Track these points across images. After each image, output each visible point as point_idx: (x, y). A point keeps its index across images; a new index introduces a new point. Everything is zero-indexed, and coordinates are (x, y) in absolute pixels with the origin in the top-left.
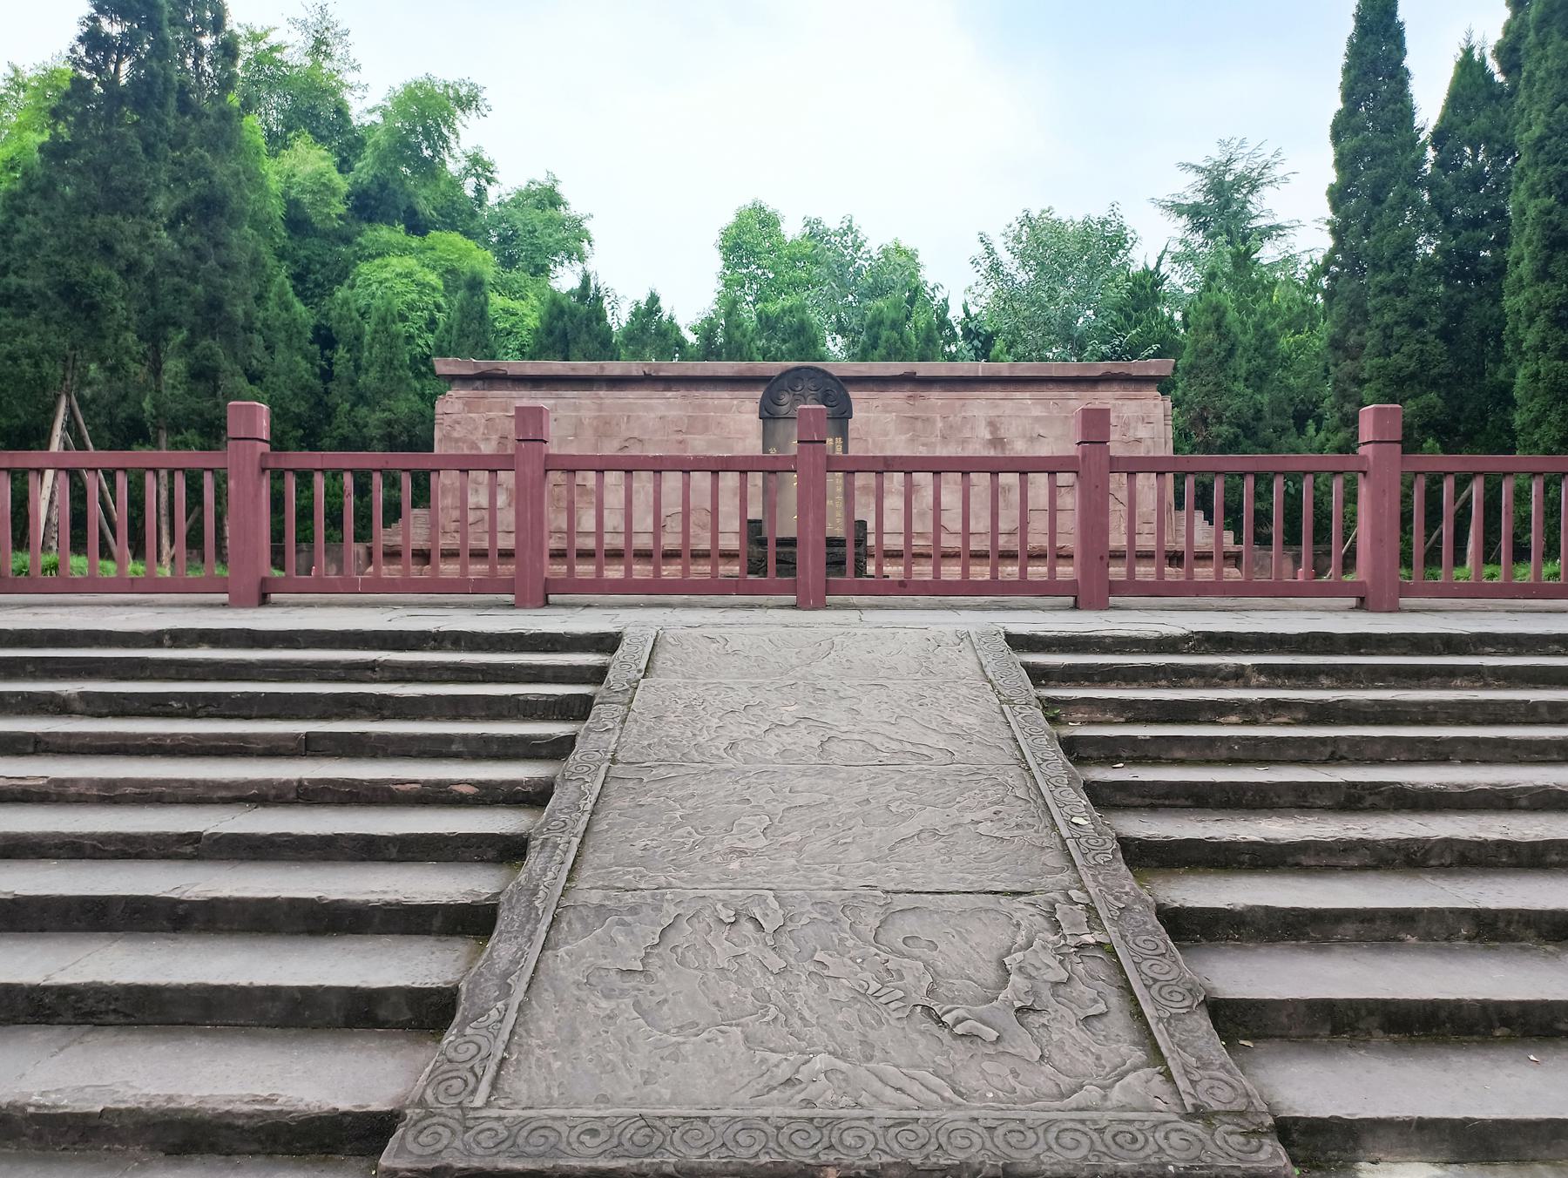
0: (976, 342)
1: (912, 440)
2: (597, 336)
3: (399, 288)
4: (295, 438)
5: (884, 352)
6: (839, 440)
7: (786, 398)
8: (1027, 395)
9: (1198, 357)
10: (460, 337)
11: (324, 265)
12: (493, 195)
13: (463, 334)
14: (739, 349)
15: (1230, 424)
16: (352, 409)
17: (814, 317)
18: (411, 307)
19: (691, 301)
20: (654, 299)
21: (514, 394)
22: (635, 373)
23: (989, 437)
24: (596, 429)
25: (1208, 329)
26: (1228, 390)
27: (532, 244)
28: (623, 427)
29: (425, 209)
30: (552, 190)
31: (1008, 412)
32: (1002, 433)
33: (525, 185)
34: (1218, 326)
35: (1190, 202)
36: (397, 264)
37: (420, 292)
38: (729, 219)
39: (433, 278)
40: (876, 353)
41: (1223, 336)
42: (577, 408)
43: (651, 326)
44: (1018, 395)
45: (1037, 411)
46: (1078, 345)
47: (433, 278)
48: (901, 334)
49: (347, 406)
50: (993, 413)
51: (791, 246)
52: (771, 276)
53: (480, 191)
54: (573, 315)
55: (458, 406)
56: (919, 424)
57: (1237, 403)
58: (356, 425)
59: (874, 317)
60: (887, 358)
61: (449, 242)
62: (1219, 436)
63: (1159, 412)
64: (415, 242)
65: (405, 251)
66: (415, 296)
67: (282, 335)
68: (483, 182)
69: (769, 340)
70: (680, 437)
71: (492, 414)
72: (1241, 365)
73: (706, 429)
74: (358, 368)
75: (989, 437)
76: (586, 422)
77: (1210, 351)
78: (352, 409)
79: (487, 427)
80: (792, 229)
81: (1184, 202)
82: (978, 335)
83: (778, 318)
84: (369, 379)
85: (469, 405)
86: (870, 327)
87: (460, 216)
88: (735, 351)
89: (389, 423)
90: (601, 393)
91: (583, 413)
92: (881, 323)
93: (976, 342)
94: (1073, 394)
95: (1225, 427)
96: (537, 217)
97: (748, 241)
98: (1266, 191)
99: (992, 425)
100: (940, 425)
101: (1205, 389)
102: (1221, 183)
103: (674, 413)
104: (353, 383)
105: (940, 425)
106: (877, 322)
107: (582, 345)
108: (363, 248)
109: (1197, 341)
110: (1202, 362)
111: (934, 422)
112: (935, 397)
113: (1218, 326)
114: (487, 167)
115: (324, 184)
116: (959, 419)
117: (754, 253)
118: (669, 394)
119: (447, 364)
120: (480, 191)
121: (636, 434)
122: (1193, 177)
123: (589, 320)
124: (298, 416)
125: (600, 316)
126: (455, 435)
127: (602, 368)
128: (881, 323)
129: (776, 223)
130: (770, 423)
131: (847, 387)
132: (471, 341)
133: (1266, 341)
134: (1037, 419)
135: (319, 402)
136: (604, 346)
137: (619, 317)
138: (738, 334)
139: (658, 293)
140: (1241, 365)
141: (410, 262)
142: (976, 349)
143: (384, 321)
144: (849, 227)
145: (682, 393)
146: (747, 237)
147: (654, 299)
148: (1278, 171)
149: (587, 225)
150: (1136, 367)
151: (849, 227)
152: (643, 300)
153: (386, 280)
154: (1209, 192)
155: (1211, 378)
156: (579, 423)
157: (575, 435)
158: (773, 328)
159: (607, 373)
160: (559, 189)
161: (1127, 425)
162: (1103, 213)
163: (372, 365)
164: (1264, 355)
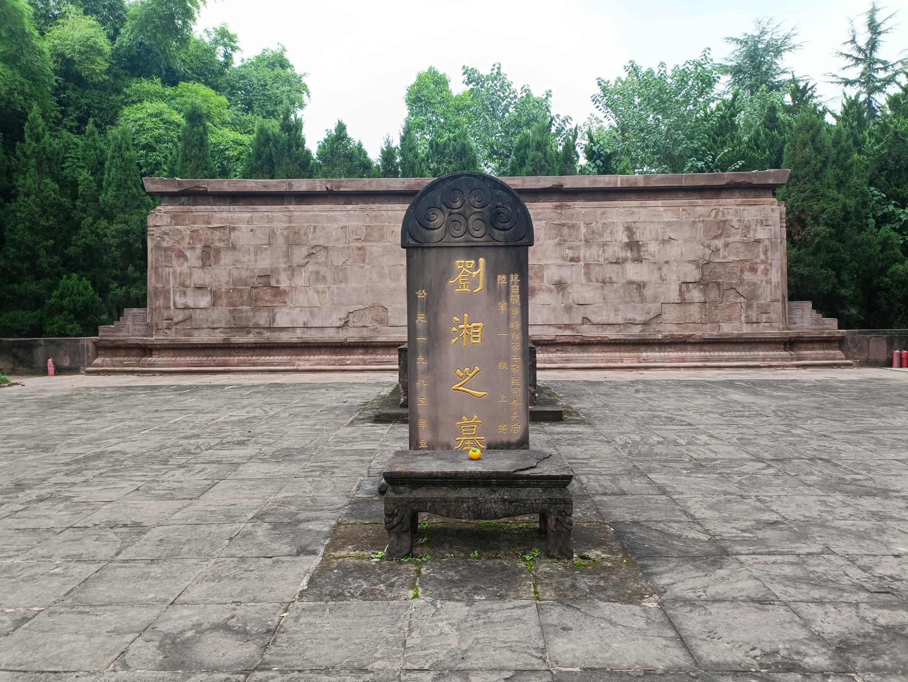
0: (598, 162)
1: (559, 244)
2: (297, 159)
3: (149, 125)
4: (45, 248)
5: (530, 169)
6: (515, 278)
7: (438, 219)
8: (659, 203)
9: (796, 168)
10: (184, 161)
11: (101, 110)
12: (237, 61)
13: (186, 159)
14: (412, 168)
15: (827, 224)
16: (94, 222)
17: (473, 142)
18: (158, 140)
19: (378, 130)
20: (341, 128)
21: (215, 208)
22: (319, 189)
23: (626, 240)
24: (287, 238)
25: (804, 145)
26: (824, 196)
27: (264, 95)
28: (310, 236)
29: (179, 66)
30: (281, 56)
31: (642, 219)
32: (637, 237)
33: (260, 51)
34: (813, 141)
35: (734, 63)
36: (150, 107)
37: (166, 129)
38: (413, 80)
39: (178, 118)
40: (525, 169)
41: (818, 150)
42: (270, 220)
43: (341, 152)
44: (652, 203)
45: (669, 217)
46: (676, 164)
47: (178, 118)
48: (545, 153)
49: (90, 219)
50: (630, 219)
51: (456, 99)
52: (442, 120)
53: (227, 56)
54: (277, 142)
55: (166, 219)
56: (565, 231)
57: (832, 207)
58: (97, 235)
59: (521, 141)
60: (533, 173)
61: (198, 93)
62: (817, 235)
63: (776, 216)
64: (169, 91)
65: (162, 97)
66: (162, 131)
67: (33, 161)
68: (229, 51)
69: (439, 163)
70: (359, 245)
71: (196, 227)
72: (830, 173)
73: (382, 238)
74: (100, 185)
75: (626, 240)
76: (278, 232)
77: (808, 163)
78: (94, 222)
79: (191, 237)
80: (458, 87)
81: (730, 64)
82: (600, 156)
83: (445, 145)
84: (107, 197)
85: (176, 218)
86: (518, 149)
87: (210, 72)
88: (410, 170)
89: (127, 233)
90: (291, 207)
91: (275, 224)
92: (527, 146)
93: (598, 162)
94: (700, 201)
95: (821, 228)
96: (268, 74)
97: (425, 95)
98: (786, 55)
99: (629, 230)
100: (583, 230)
101: (803, 195)
102: (757, 49)
103: (353, 224)
104: (97, 200)
105: (583, 230)
106: (524, 145)
107: (284, 166)
108: (128, 96)
109: (795, 155)
110: (802, 172)
111: (578, 228)
112: (579, 207)
113: (813, 141)
114: (232, 38)
115: (91, 47)
116: (600, 225)
117: (429, 103)
118: (349, 207)
119: (154, 183)
120: (227, 56)
121: (321, 243)
122: (734, 46)
123: (290, 147)
124: (49, 228)
125: (299, 142)
126: (165, 244)
127: (290, 185)
128: (527, 146)
129: (446, 83)
130: (417, 254)
131: (522, 198)
132: (193, 165)
133: (843, 155)
134: (668, 224)
135: (68, 218)
136: (303, 165)
137: (313, 140)
138: (410, 155)
139: (345, 122)
140: (830, 173)
141: (163, 106)
142: (598, 166)
143: (120, 148)
144: (498, 73)
145: (361, 206)
146: (425, 92)
147: (341, 128)
148: (794, 41)
149: (305, 80)
150: (755, 176)
151: (498, 73)
152: (332, 127)
153: (140, 119)
154: (745, 57)
155: (808, 185)
156: (272, 234)
157: (269, 244)
158: (442, 153)
159: (295, 189)
160: (287, 56)
161: (747, 228)
162: (697, 56)
163: (110, 185)
164: (841, 167)
